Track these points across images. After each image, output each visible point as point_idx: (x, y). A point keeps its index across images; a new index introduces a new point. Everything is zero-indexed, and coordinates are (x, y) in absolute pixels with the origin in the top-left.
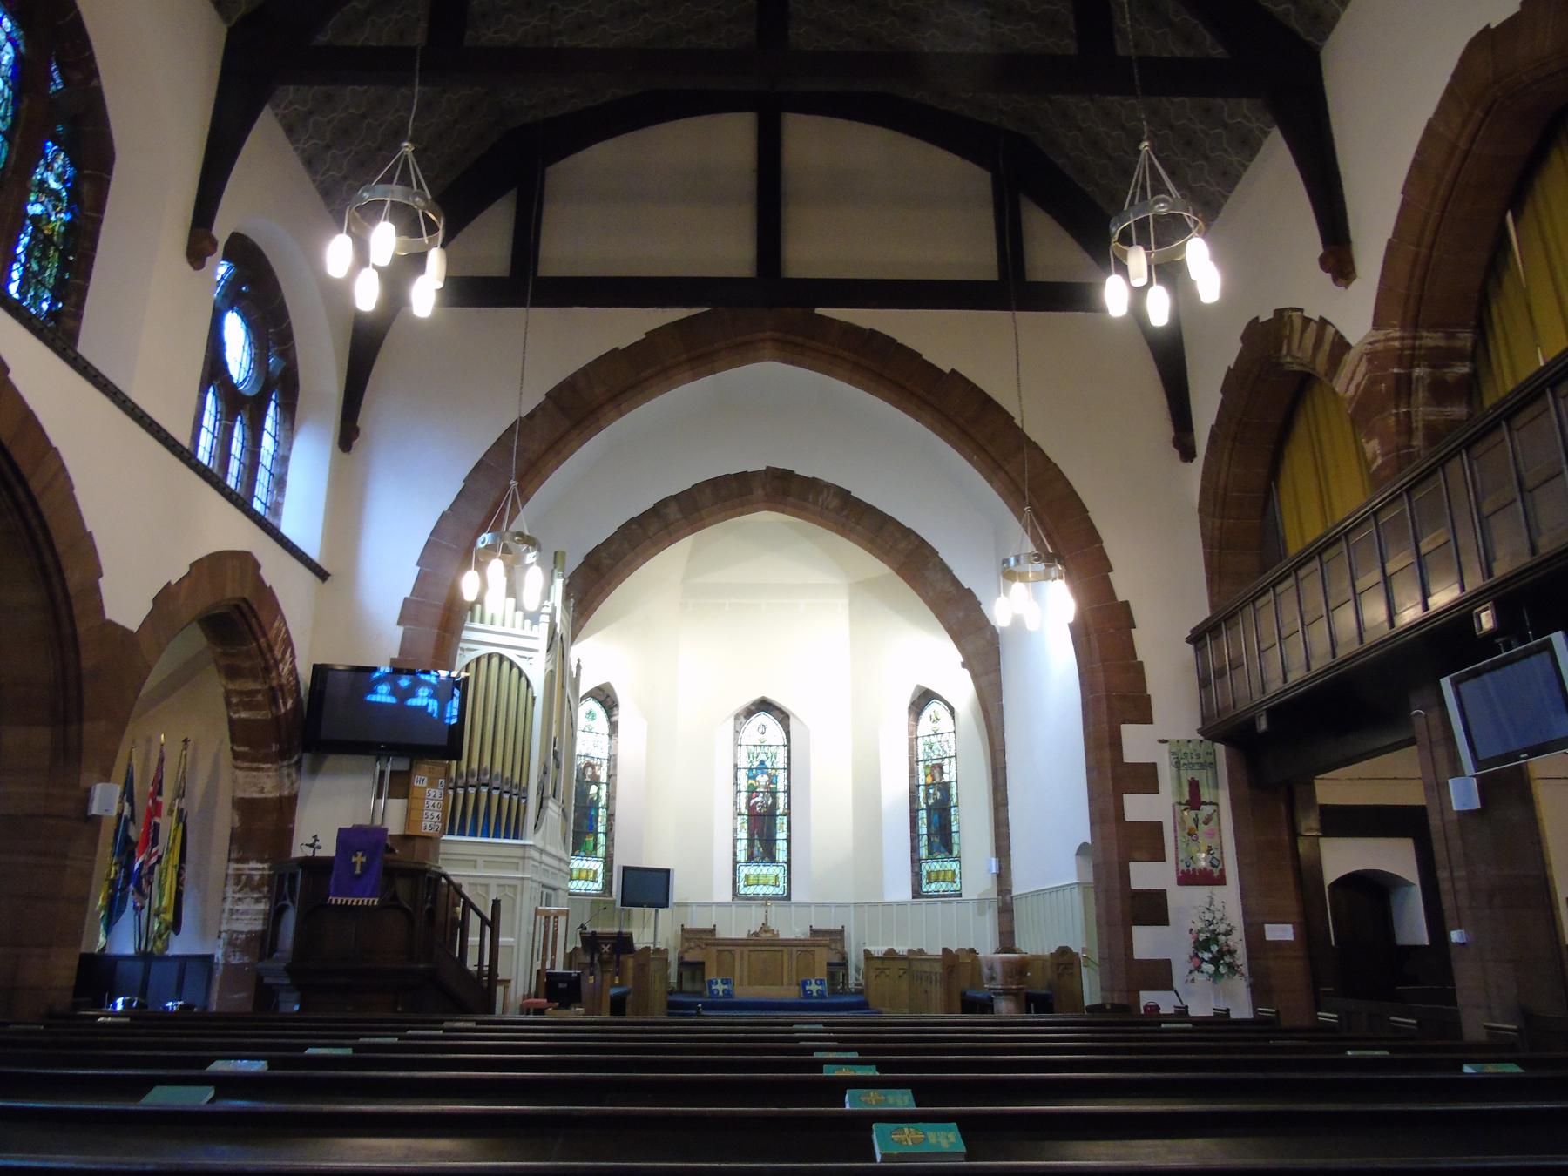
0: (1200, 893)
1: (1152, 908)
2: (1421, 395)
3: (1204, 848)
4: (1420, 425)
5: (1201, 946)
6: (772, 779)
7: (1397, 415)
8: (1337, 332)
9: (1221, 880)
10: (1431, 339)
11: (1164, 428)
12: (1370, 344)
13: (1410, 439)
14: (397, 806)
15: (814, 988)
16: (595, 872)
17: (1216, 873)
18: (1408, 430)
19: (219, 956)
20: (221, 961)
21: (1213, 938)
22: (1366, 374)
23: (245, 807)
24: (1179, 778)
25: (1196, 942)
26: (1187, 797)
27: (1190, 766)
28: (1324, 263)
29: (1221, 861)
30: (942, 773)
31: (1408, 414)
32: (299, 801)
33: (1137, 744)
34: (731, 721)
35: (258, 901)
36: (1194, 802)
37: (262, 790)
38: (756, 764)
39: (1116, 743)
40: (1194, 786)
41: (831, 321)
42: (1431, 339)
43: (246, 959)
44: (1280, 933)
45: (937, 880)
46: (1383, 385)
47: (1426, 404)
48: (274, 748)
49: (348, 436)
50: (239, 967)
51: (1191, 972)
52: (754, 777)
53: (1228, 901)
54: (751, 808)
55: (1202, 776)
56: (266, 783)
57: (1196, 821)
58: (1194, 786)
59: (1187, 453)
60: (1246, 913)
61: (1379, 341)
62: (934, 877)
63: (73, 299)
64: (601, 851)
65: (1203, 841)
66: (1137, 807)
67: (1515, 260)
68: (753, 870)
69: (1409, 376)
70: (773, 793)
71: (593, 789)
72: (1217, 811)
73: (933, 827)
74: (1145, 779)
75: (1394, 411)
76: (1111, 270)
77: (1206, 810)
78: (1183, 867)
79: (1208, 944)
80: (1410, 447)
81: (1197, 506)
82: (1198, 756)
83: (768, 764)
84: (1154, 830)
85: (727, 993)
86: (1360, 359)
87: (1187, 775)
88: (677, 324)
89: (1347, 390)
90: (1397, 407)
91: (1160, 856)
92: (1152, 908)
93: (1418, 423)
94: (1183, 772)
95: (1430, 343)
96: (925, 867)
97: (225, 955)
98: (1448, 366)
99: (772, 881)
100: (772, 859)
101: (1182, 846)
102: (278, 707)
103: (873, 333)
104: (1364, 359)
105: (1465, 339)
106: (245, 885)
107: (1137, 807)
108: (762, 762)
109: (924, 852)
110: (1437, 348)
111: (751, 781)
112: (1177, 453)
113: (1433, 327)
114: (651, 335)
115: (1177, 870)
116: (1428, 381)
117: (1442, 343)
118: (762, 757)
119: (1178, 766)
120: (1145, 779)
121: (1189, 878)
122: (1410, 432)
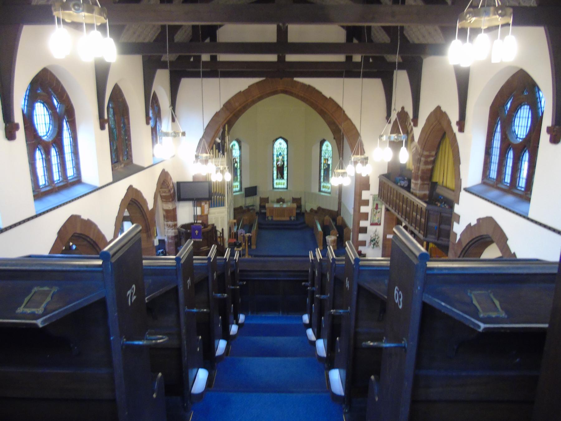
0: (374, 228)
1: (364, 230)
2: (422, 163)
5: (371, 241)
6: (283, 158)
11: (385, 114)
14: (199, 209)
15: (293, 218)
16: (238, 186)
19: (166, 240)
20: (167, 241)
21: (374, 240)
23: (167, 211)
26: (375, 207)
27: (377, 200)
30: (328, 161)
32: (177, 209)
33: (366, 195)
34: (272, 142)
35: (172, 230)
36: (377, 208)
37: (169, 208)
38: (279, 153)
39: (360, 195)
40: (377, 205)
41: (298, 82)
42: (426, 153)
43: (172, 241)
45: (325, 188)
48: (171, 200)
49: (173, 120)
50: (171, 243)
52: (278, 157)
53: (380, 229)
54: (277, 166)
56: (170, 206)
58: (377, 205)
62: (324, 187)
63: (129, 148)
64: (239, 180)
65: (377, 217)
66: (363, 209)
68: (278, 181)
70: (283, 161)
71: (236, 165)
73: (325, 175)
74: (366, 203)
77: (379, 210)
78: (372, 222)
79: (374, 242)
83: (282, 153)
84: (367, 214)
85: (272, 220)
87: (375, 203)
88: (257, 84)
91: (367, 219)
92: (364, 230)
93: (421, 169)
94: (375, 202)
96: (322, 184)
97: (168, 240)
99: (283, 184)
100: (282, 177)
101: (372, 218)
102: (171, 192)
103: (309, 86)
105: (433, 153)
106: (169, 226)
107: (363, 209)
108: (280, 153)
109: (322, 180)
111: (278, 158)
113: (427, 151)
114: (250, 87)
118: (280, 151)
120: (366, 203)
121: (372, 224)
122: (419, 170)
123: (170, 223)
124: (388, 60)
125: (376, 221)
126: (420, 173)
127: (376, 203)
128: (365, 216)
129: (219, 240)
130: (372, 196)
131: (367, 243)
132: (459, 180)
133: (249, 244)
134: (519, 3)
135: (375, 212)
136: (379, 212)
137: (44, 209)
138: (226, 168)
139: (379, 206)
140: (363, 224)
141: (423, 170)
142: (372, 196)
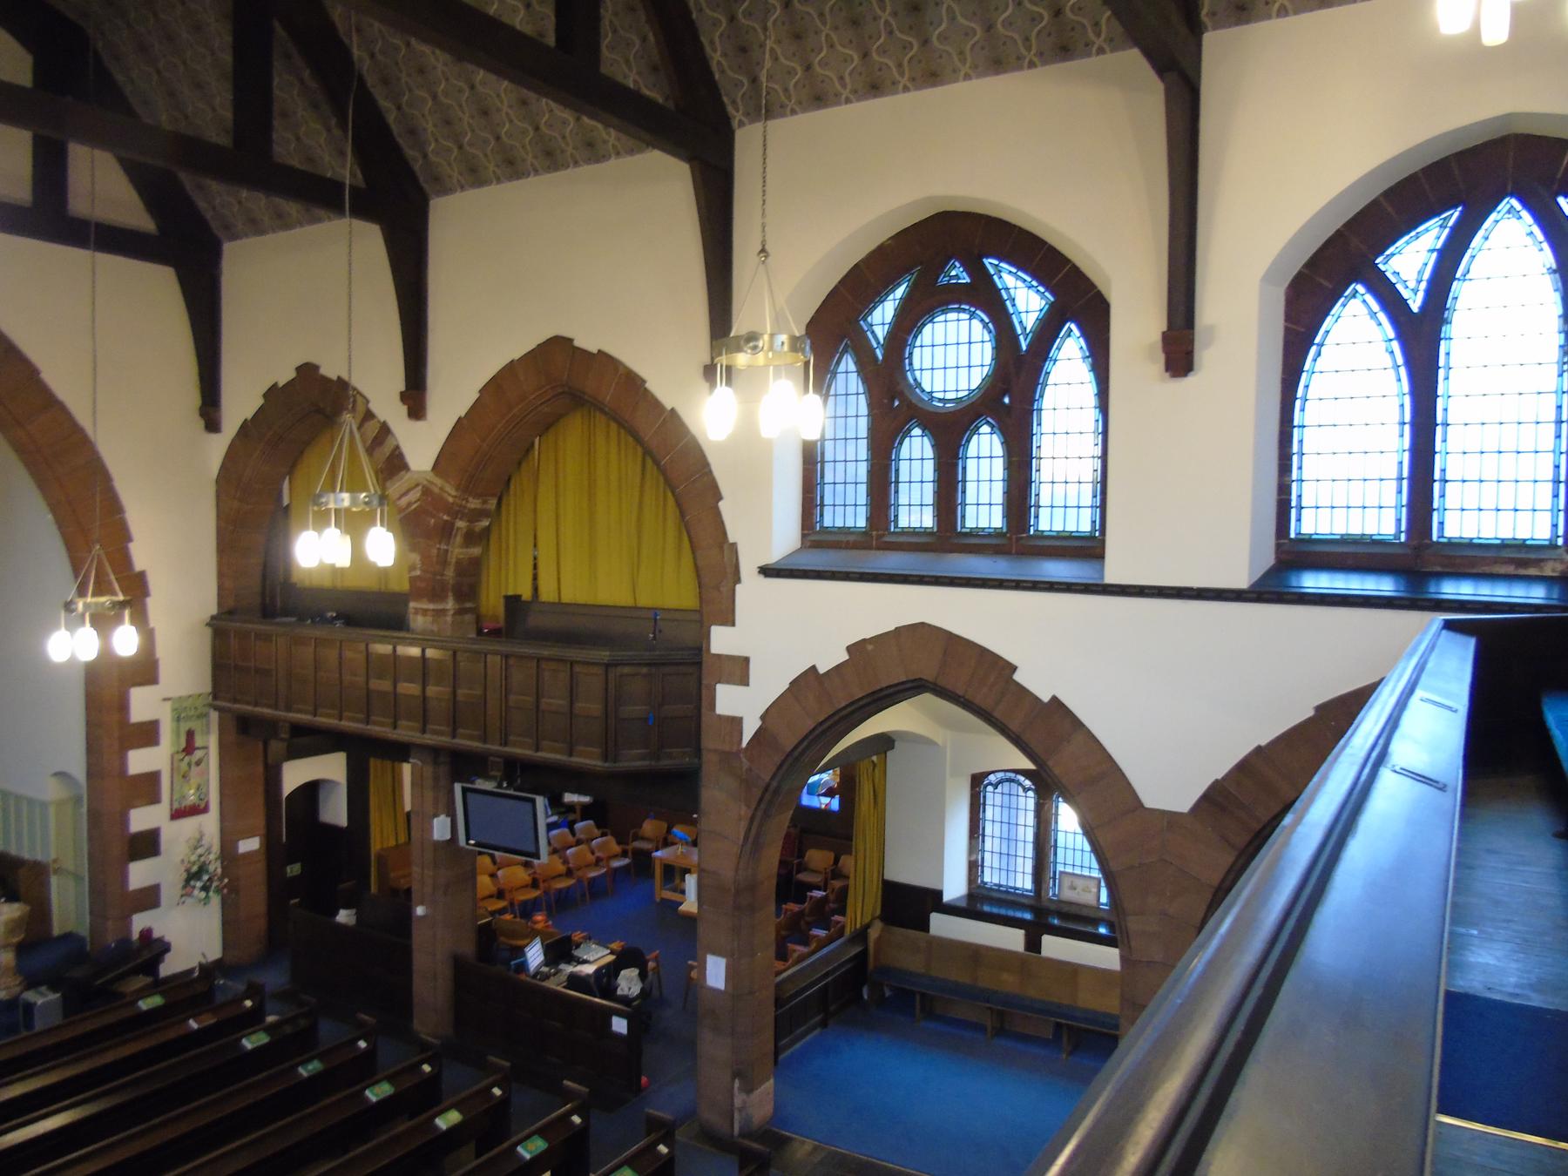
0: (189, 825)
1: (147, 845)
3: (194, 785)
4: (454, 560)
7: (439, 549)
8: (397, 447)
9: (205, 810)
10: (474, 504)
11: (192, 397)
12: (429, 481)
13: (444, 570)
17: (202, 806)
18: (443, 560)
22: (419, 500)
24: (178, 728)
25: (188, 871)
26: (183, 745)
27: (188, 718)
28: (404, 397)
29: (207, 794)
31: (447, 551)
36: (189, 749)
40: (190, 735)
44: (250, 845)
46: (433, 521)
47: (461, 547)
51: (182, 896)
53: (209, 824)
55: (195, 725)
57: (189, 765)
58: (190, 735)
59: (212, 425)
60: (223, 832)
61: (436, 485)
65: (194, 781)
66: (140, 761)
67: (534, 458)
69: (453, 524)
72: (207, 754)
74: (147, 734)
75: (438, 546)
76: (308, 525)
77: (198, 754)
78: (176, 806)
80: (442, 575)
81: (215, 477)
82: (196, 708)
84: (153, 778)
86: (417, 485)
87: (185, 727)
89: (400, 498)
90: (440, 543)
91: (155, 799)
92: (147, 845)
95: (473, 506)
98: (480, 521)
101: (177, 787)
104: (420, 488)
105: (492, 503)
107: (140, 761)
110: (475, 509)
112: (201, 423)
113: (477, 496)
115: (171, 809)
116: (465, 530)
117: (479, 506)
119: (178, 719)
120: (147, 734)
121: (177, 814)
123: (660, 843)
124: (605, 69)
125: (191, 797)
126: (450, 573)
127: (187, 729)
128: (147, 787)
129: (303, 1023)
130: (168, 705)
131: (166, 895)
132: (721, 548)
133: (1102, 930)
134: (578, 119)
135: (184, 765)
136: (198, 763)
137: (1377, 721)
138: (1207, 14)
139: (199, 742)
140: (141, 819)
141: (459, 563)
142: (168, 706)
